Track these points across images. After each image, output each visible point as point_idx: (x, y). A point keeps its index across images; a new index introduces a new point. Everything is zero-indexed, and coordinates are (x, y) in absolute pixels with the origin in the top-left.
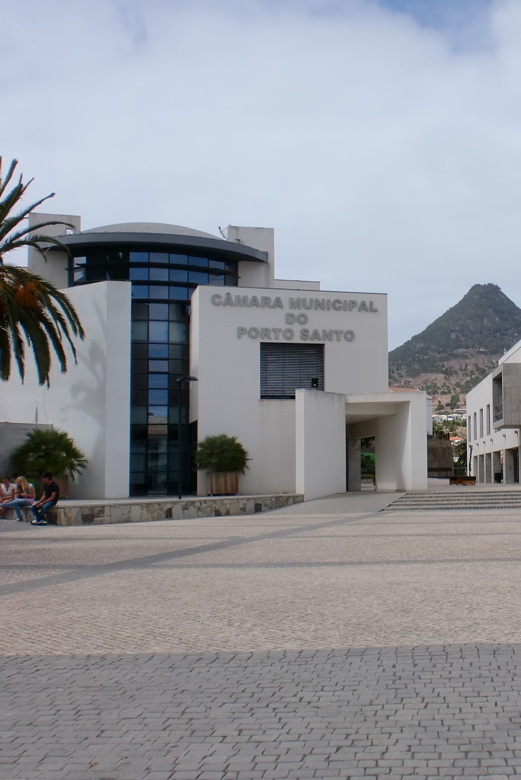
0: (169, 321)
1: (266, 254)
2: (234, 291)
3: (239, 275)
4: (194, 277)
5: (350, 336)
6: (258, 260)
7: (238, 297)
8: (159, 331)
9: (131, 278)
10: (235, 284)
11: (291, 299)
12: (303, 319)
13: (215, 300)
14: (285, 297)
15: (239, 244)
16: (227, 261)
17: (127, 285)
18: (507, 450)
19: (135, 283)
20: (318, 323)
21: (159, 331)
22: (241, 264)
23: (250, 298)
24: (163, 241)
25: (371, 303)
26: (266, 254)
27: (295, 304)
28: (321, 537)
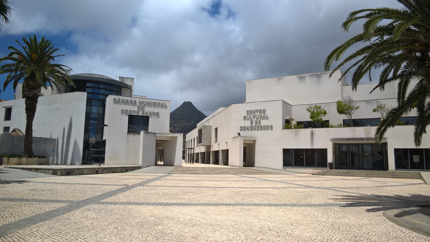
0: (98, 106)
1: (131, 86)
2: (121, 98)
4: (107, 92)
5: (157, 115)
6: (129, 88)
9: (87, 90)
10: (120, 95)
11: (139, 101)
12: (143, 108)
14: (137, 100)
16: (118, 88)
19: (88, 93)
20: (148, 110)
21: (95, 110)
22: (123, 89)
24: (94, 79)
26: (131, 86)
27: (141, 103)
28: (230, 205)
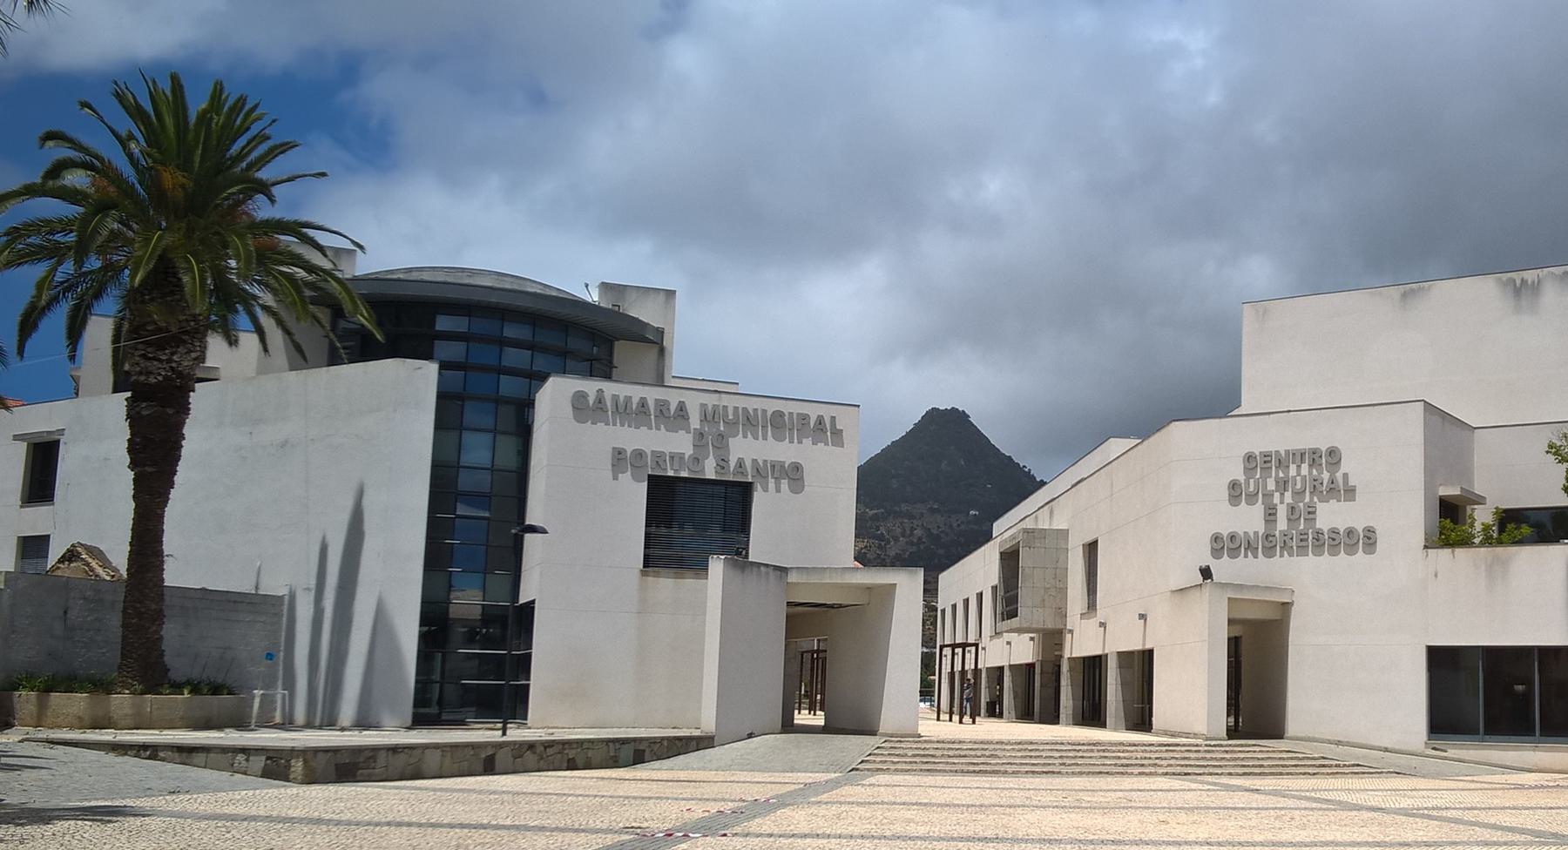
0: (494, 431)
2: (610, 389)
3: (615, 362)
4: (540, 363)
5: (794, 475)
6: (652, 340)
7: (615, 398)
8: (477, 451)
10: (608, 376)
11: (703, 406)
13: (583, 409)
15: (618, 313)
16: (595, 338)
17: (431, 369)
18: (1286, 607)
19: (444, 366)
20: (746, 450)
22: (619, 346)
23: (635, 401)
25: (833, 418)
27: (708, 416)
